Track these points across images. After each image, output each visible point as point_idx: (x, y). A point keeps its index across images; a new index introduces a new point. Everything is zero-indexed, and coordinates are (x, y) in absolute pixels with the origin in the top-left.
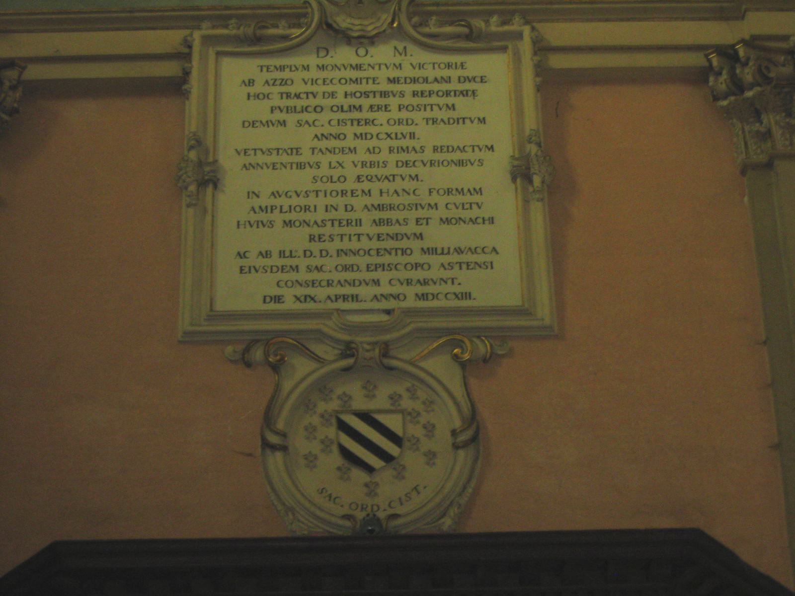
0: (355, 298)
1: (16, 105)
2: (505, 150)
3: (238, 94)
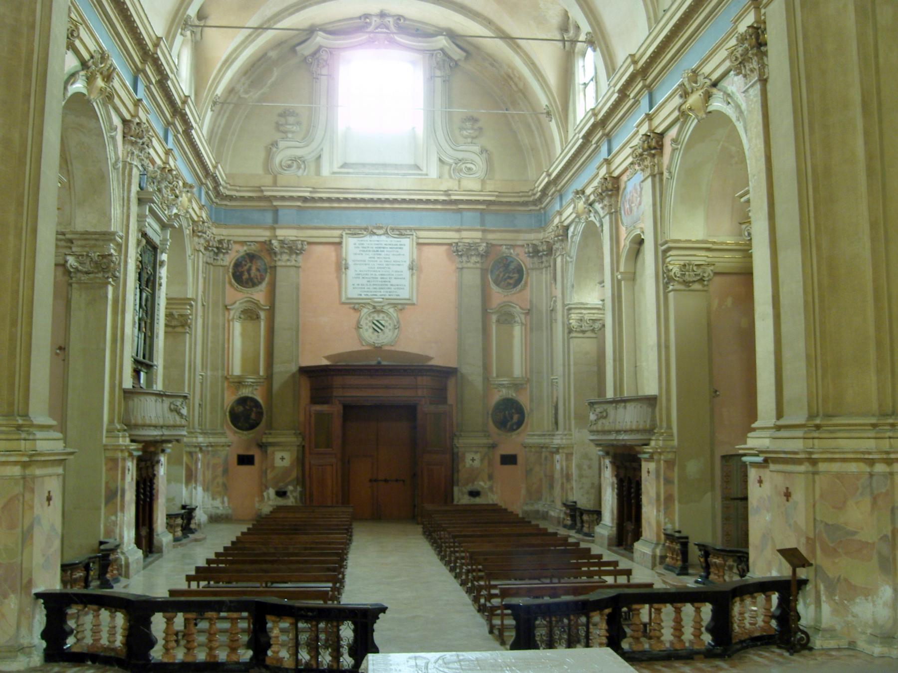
0: (147, 300)
1: (368, 20)
2: (408, 263)
3: (351, 244)
